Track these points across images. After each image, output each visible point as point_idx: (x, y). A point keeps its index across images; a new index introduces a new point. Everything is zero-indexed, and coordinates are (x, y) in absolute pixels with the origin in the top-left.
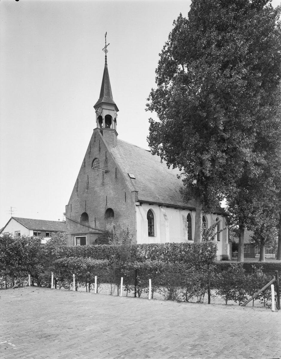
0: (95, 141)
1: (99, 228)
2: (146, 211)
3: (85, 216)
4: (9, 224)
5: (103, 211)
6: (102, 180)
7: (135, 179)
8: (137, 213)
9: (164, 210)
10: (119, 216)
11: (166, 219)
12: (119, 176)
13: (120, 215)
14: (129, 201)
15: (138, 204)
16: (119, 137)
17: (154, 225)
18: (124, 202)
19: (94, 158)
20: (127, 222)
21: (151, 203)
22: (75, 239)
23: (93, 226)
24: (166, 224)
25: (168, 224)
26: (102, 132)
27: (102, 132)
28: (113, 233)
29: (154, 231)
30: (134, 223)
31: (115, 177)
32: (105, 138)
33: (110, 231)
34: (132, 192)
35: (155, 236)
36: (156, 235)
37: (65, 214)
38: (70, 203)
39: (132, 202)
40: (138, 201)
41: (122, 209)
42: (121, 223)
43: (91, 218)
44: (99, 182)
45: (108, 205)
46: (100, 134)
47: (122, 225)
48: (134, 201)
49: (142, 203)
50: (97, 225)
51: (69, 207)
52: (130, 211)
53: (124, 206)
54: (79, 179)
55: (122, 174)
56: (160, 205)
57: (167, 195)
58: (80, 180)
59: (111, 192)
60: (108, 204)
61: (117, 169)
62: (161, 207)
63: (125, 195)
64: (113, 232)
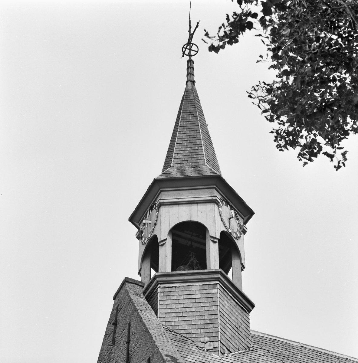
27: (151, 298)
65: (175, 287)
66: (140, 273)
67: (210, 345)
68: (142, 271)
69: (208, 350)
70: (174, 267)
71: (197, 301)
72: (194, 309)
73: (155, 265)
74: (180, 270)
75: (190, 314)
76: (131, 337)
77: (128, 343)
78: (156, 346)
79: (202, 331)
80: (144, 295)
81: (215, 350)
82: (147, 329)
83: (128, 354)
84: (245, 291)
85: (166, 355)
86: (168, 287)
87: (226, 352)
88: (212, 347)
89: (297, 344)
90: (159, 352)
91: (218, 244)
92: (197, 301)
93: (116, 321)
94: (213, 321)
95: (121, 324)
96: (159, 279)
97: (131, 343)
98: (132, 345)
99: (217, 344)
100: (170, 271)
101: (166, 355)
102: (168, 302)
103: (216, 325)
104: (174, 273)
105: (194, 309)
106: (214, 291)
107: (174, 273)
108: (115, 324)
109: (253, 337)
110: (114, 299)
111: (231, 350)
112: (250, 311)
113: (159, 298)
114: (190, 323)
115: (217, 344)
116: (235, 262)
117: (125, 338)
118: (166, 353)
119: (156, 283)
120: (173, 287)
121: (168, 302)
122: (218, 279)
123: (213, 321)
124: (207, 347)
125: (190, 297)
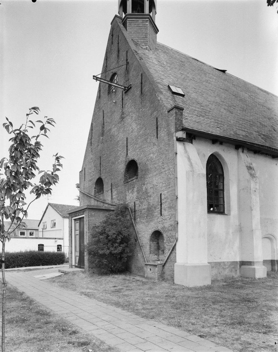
0: (112, 43)
1: (116, 201)
2: (204, 156)
3: (100, 182)
4: (46, 212)
5: (122, 167)
6: (121, 111)
7: (183, 96)
8: (178, 156)
9: (246, 158)
10: (147, 171)
11: (253, 176)
12: (146, 89)
13: (148, 169)
14: (162, 134)
15: (181, 134)
16: (161, 38)
17: (223, 190)
18: (154, 140)
19: (111, 75)
20: (160, 181)
21: (215, 140)
22: (73, 221)
23: (109, 199)
24: (253, 185)
25: (258, 188)
26: (125, 24)
27: (125, 24)
28: (136, 208)
29: (224, 202)
30: (172, 182)
31: (140, 93)
32: (131, 33)
33: (131, 205)
34: (168, 112)
35: (226, 212)
36: (229, 211)
37: (78, 186)
38: (84, 168)
39: (170, 134)
40: (184, 129)
41: (152, 155)
42: (149, 186)
43: (107, 187)
44: (117, 116)
45: (129, 154)
46: (121, 26)
47: (152, 190)
48: (173, 130)
49: (192, 136)
50: (114, 197)
51: (83, 173)
52: (166, 157)
53: (155, 149)
54: (93, 123)
55: (153, 83)
56: (239, 145)
57: (255, 132)
58: (94, 124)
59: (134, 126)
60: (129, 152)
61: (143, 74)
62: (240, 150)
63: (157, 122)
64: (137, 206)
65: (133, 20)
66: (119, 13)
67: (145, 47)
68: (120, 12)
69: (144, 49)
70: (132, 11)
71: (141, 27)
72: (139, 31)
73: (125, 10)
74: (134, 13)
75: (138, 33)
76: (119, 41)
77: (118, 44)
78: (130, 46)
79: (142, 41)
80: (122, 22)
81: (146, 49)
82: (126, 38)
83: (118, 48)
84: (156, 23)
85: (134, 50)
86: (131, 20)
87: (150, 50)
88: (145, 48)
89: (170, 48)
90: (131, 48)
91: (122, 9)
92: (141, 27)
93: (113, 34)
94: (146, 37)
95: (115, 36)
96: (128, 16)
97: (119, 44)
98: (120, 45)
99: (147, 46)
100: (131, 12)
101: (134, 50)
102: (131, 27)
103: (147, 39)
104: (133, 14)
105: (139, 31)
106: (147, 23)
107: (133, 14)
108: (112, 35)
109: (157, 44)
110: (111, 24)
111: (151, 49)
112: (157, 33)
113: (128, 25)
114: (138, 37)
115: (147, 46)
116: (153, 10)
117: (117, 42)
118: (134, 49)
119: (148, 17)
120: (132, 20)
121: (131, 27)
122: (148, 18)
123: (146, 37)
124: (144, 48)
125: (138, 25)
